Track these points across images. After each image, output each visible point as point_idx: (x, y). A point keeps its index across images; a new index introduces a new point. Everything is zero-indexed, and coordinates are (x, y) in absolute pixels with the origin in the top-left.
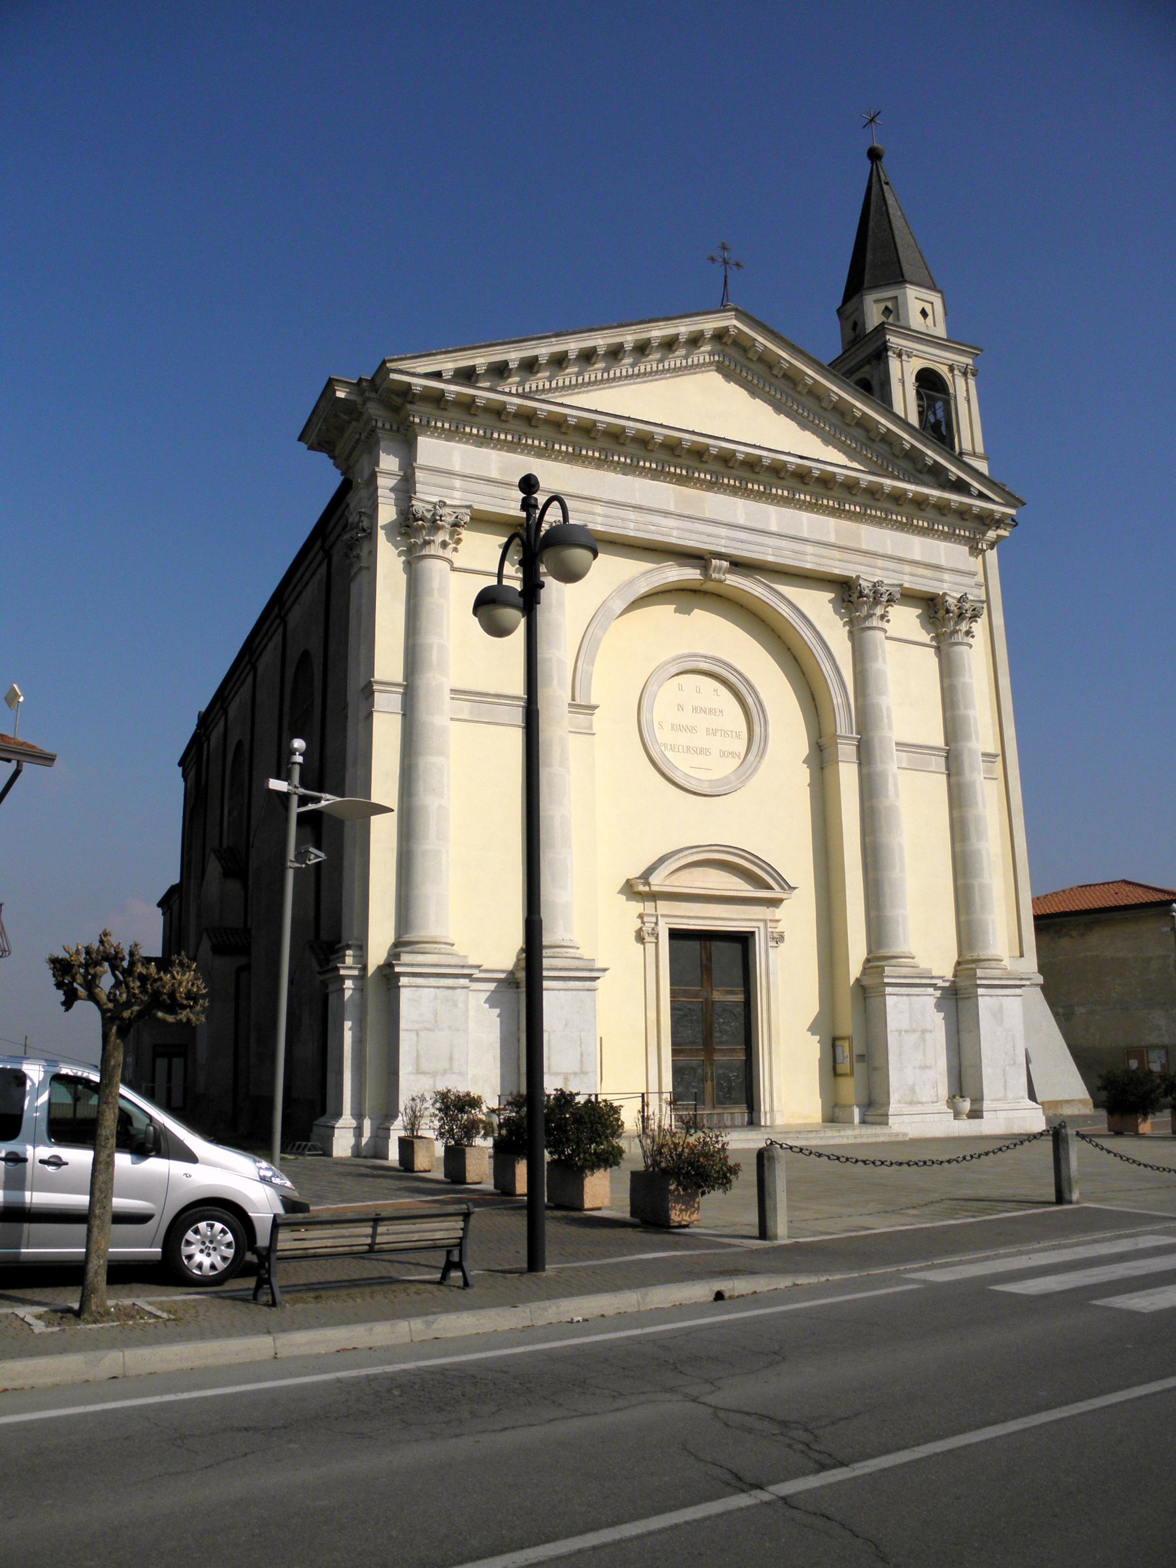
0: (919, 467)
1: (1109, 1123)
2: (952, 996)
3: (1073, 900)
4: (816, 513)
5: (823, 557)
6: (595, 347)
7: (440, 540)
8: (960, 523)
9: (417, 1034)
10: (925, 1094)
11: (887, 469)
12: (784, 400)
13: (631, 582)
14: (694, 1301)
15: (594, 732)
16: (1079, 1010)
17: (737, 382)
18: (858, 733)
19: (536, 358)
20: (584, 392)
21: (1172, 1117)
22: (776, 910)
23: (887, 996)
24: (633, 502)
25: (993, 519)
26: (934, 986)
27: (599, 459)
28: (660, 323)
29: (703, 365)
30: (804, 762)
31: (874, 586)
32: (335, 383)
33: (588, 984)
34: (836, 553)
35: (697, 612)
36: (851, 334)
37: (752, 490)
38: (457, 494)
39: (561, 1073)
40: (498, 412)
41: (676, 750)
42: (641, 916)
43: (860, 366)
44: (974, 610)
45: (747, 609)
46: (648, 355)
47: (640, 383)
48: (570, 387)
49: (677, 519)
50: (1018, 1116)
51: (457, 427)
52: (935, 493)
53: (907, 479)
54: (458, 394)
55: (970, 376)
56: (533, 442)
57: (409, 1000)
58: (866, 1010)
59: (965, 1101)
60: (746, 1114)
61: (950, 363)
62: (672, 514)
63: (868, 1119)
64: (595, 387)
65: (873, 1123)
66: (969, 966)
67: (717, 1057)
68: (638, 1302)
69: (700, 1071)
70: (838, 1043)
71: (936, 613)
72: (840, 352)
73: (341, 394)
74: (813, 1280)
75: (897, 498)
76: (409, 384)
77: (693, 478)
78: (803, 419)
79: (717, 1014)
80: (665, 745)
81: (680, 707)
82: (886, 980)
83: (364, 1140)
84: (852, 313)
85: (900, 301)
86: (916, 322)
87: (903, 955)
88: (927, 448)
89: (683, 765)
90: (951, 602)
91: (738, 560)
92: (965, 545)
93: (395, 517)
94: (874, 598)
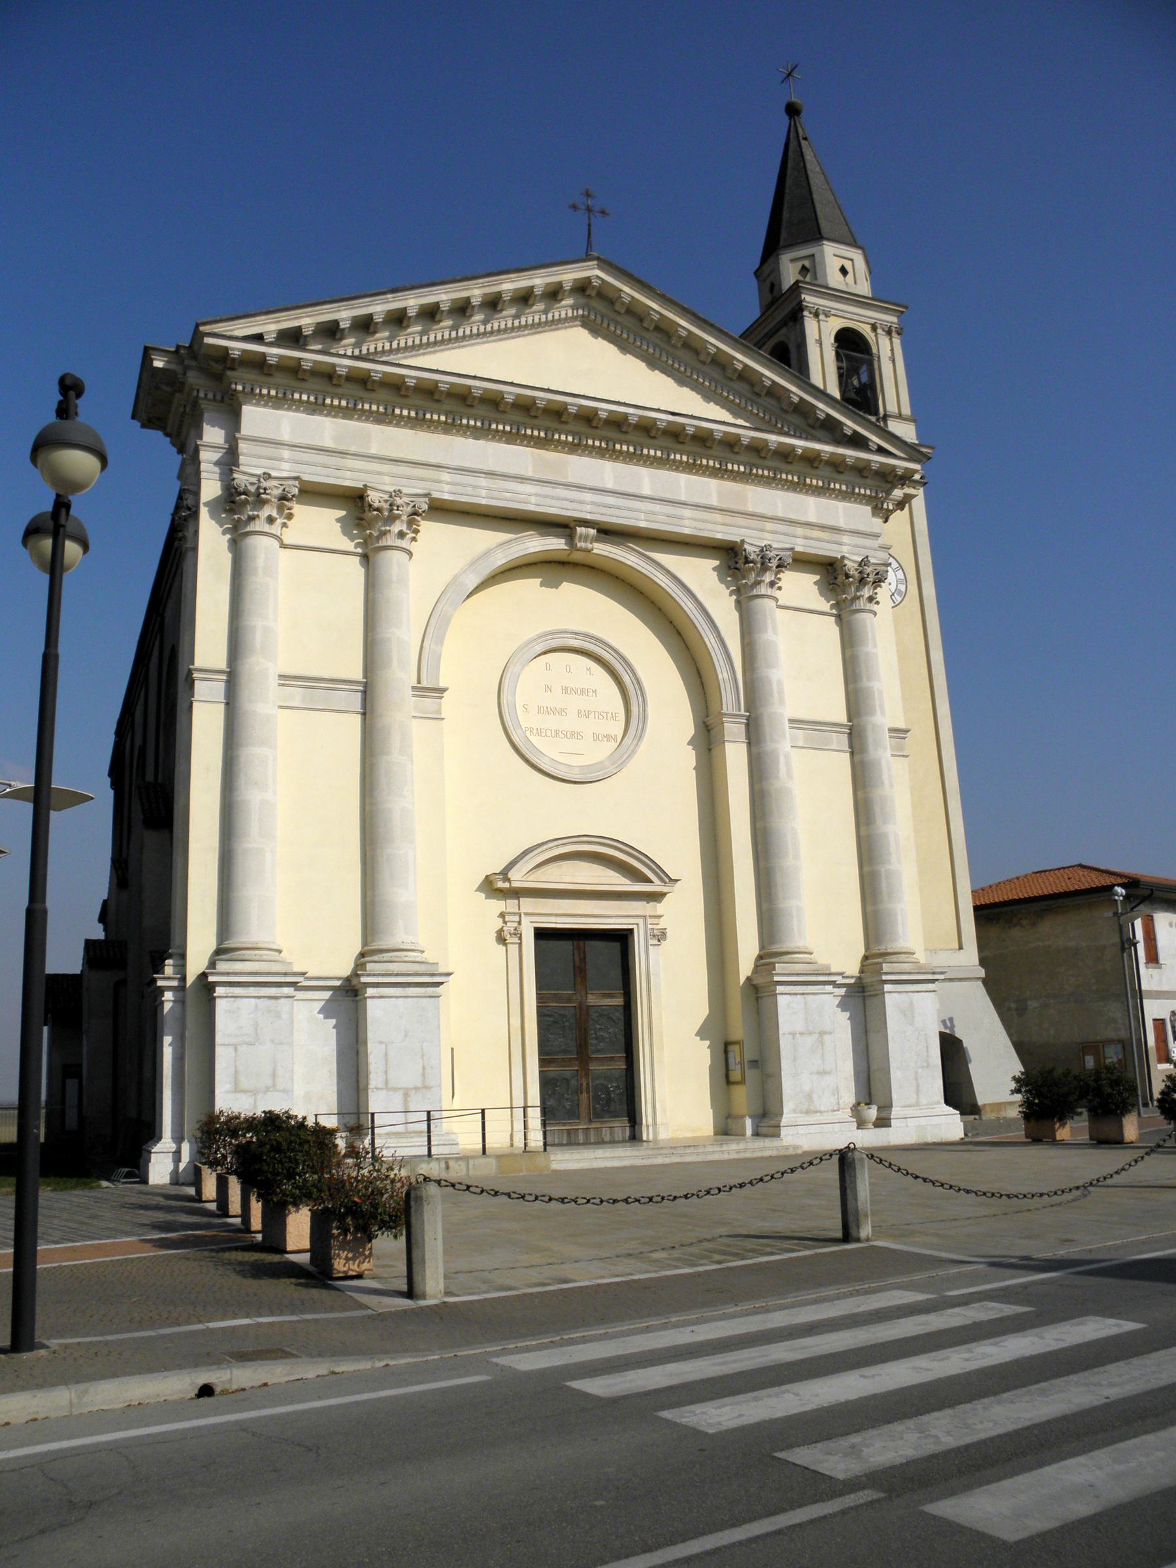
0: (810, 421)
1: (1026, 1129)
2: (858, 994)
3: (1025, 887)
4: (695, 474)
5: (703, 521)
6: (438, 303)
7: (266, 515)
8: (859, 480)
9: (236, 1049)
10: (824, 1102)
11: (776, 424)
12: (657, 354)
13: (486, 554)
14: (162, 1399)
15: (443, 716)
16: (1033, 1004)
17: (605, 337)
18: (747, 710)
19: (370, 316)
20: (430, 353)
21: (1089, 1121)
22: (658, 905)
23: (778, 996)
24: (486, 468)
25: (896, 475)
26: (833, 983)
27: (446, 423)
28: (512, 276)
29: (566, 319)
30: (689, 744)
31: (762, 551)
32: (151, 352)
33: (430, 991)
34: (718, 517)
35: (566, 586)
36: (769, 297)
37: (621, 452)
38: (285, 466)
39: (400, 1089)
40: (328, 376)
41: (544, 734)
42: (502, 915)
43: (775, 331)
44: (877, 574)
45: (623, 581)
46: (501, 311)
47: (494, 341)
48: (413, 347)
49: (536, 485)
50: (932, 1123)
51: (285, 394)
52: (827, 449)
53: (792, 433)
54: (281, 357)
55: (894, 335)
56: (370, 407)
57: (226, 1011)
58: (758, 1011)
59: (870, 1108)
60: (628, 1128)
61: (873, 321)
62: (530, 480)
63: (763, 1130)
64: (443, 347)
65: (766, 1136)
66: (876, 960)
67: (593, 1067)
68: (71, 1403)
69: (573, 1082)
70: (730, 1048)
71: (836, 578)
72: (756, 314)
73: (158, 364)
74: (364, 1365)
75: (785, 455)
76: (226, 349)
77: (552, 440)
78: (680, 375)
79: (593, 1020)
80: (531, 730)
81: (548, 688)
82: (776, 978)
83: (182, 1166)
84: (769, 275)
85: (817, 260)
86: (834, 279)
87: (797, 950)
88: (818, 400)
89: (550, 752)
90: (851, 566)
91: (606, 527)
92: (867, 505)
93: (219, 492)
94: (763, 564)
